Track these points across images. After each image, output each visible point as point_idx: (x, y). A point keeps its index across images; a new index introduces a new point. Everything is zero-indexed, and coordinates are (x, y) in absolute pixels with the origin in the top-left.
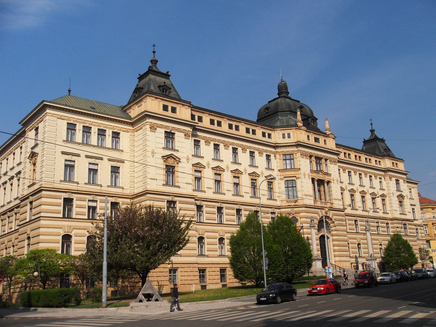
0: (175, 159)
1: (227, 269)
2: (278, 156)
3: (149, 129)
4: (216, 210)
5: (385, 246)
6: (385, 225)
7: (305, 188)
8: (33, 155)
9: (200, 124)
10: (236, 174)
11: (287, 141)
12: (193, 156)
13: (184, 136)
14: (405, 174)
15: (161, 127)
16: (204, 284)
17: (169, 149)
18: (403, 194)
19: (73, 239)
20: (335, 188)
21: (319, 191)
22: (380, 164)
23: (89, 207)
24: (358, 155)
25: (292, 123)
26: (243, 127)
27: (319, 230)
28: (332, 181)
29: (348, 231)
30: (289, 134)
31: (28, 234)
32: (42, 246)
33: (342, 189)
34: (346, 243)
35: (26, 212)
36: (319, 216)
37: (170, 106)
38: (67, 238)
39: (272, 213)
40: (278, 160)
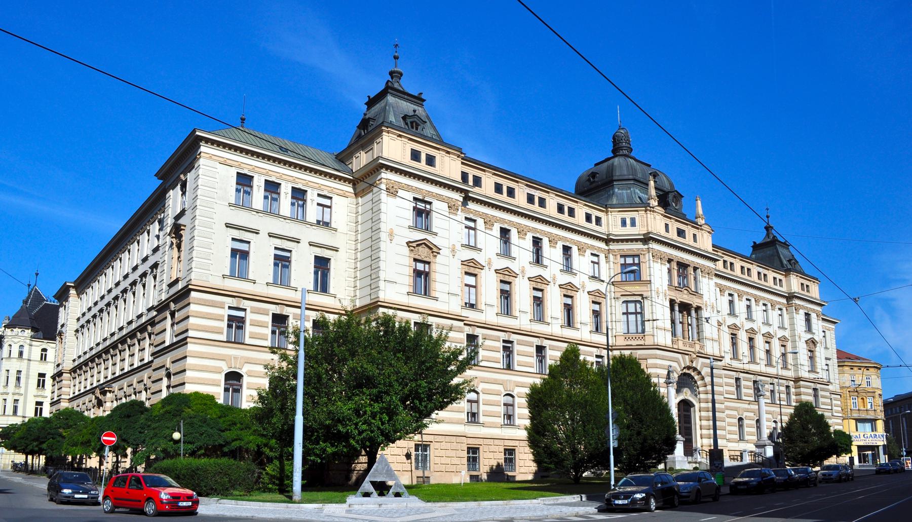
0: (431, 249)
4: (534, 350)
8: (177, 230)
9: (476, 189)
11: (629, 230)
12: (462, 246)
14: (821, 305)
15: (408, 188)
18: (816, 338)
22: (781, 286)
24: (746, 265)
26: (552, 201)
27: (678, 391)
31: (167, 369)
32: (189, 389)
35: (165, 330)
37: (424, 151)
38: (234, 378)
39: (597, 356)
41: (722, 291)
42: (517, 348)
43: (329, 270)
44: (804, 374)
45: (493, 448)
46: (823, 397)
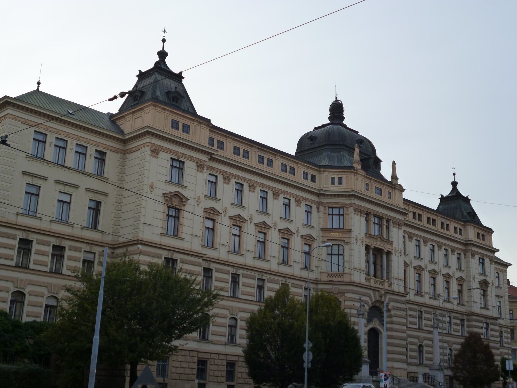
1: (240, 364)
2: (322, 208)
3: (149, 152)
5: (456, 352)
6: (459, 322)
7: (356, 256)
9: (220, 152)
10: (263, 228)
11: (337, 188)
13: (196, 168)
15: (168, 151)
16: (202, 382)
17: (174, 184)
18: (488, 279)
19: (28, 298)
20: (397, 263)
21: (375, 264)
23: (84, 261)
25: (346, 163)
27: (369, 321)
28: (393, 252)
29: (409, 326)
30: (340, 179)
33: (406, 265)
34: (404, 343)
36: (371, 299)
38: (18, 297)
40: (321, 214)
41: (410, 238)
42: (242, 280)
43: (99, 210)
44: (476, 309)
45: (218, 362)
46: (492, 330)
